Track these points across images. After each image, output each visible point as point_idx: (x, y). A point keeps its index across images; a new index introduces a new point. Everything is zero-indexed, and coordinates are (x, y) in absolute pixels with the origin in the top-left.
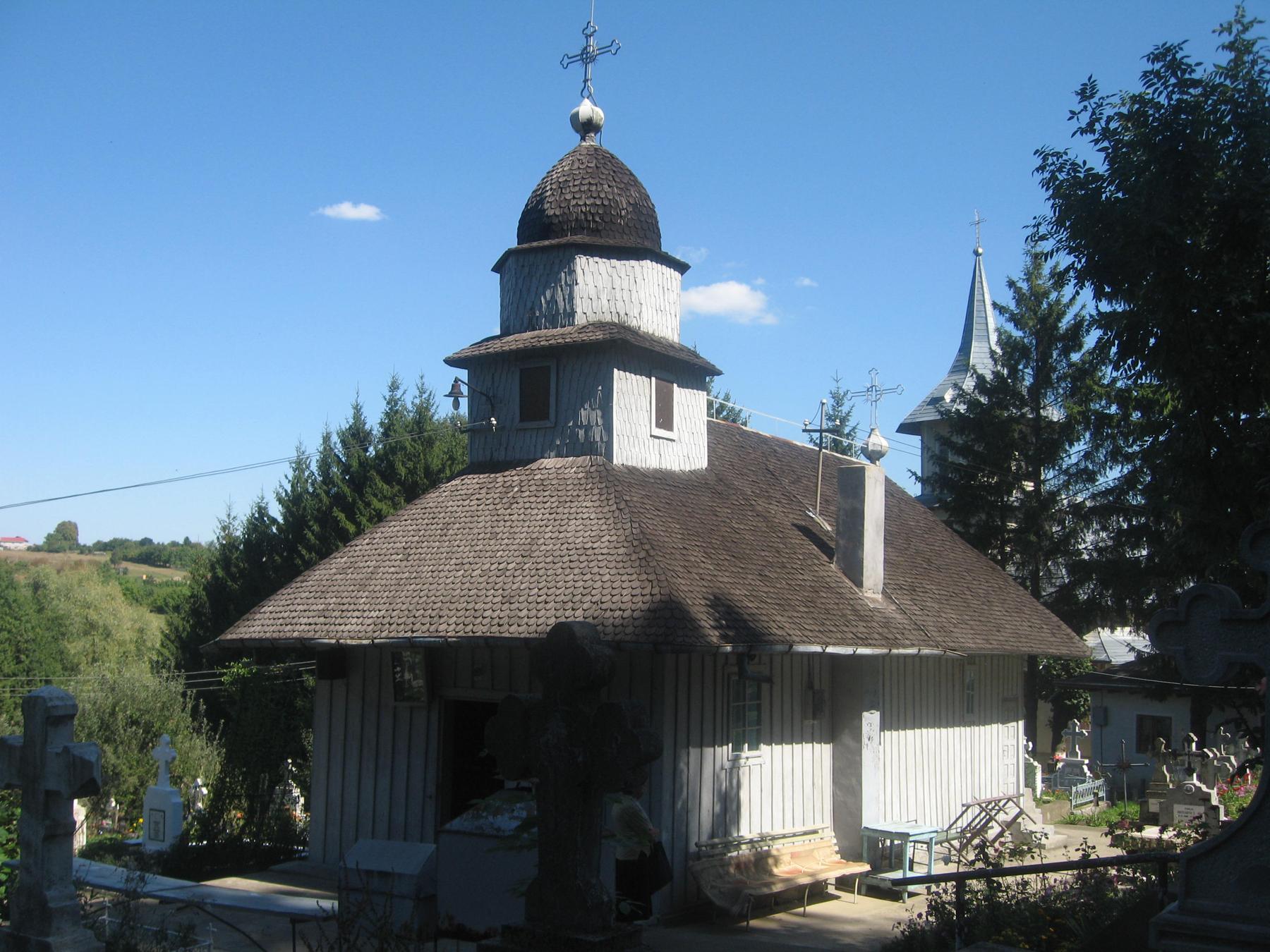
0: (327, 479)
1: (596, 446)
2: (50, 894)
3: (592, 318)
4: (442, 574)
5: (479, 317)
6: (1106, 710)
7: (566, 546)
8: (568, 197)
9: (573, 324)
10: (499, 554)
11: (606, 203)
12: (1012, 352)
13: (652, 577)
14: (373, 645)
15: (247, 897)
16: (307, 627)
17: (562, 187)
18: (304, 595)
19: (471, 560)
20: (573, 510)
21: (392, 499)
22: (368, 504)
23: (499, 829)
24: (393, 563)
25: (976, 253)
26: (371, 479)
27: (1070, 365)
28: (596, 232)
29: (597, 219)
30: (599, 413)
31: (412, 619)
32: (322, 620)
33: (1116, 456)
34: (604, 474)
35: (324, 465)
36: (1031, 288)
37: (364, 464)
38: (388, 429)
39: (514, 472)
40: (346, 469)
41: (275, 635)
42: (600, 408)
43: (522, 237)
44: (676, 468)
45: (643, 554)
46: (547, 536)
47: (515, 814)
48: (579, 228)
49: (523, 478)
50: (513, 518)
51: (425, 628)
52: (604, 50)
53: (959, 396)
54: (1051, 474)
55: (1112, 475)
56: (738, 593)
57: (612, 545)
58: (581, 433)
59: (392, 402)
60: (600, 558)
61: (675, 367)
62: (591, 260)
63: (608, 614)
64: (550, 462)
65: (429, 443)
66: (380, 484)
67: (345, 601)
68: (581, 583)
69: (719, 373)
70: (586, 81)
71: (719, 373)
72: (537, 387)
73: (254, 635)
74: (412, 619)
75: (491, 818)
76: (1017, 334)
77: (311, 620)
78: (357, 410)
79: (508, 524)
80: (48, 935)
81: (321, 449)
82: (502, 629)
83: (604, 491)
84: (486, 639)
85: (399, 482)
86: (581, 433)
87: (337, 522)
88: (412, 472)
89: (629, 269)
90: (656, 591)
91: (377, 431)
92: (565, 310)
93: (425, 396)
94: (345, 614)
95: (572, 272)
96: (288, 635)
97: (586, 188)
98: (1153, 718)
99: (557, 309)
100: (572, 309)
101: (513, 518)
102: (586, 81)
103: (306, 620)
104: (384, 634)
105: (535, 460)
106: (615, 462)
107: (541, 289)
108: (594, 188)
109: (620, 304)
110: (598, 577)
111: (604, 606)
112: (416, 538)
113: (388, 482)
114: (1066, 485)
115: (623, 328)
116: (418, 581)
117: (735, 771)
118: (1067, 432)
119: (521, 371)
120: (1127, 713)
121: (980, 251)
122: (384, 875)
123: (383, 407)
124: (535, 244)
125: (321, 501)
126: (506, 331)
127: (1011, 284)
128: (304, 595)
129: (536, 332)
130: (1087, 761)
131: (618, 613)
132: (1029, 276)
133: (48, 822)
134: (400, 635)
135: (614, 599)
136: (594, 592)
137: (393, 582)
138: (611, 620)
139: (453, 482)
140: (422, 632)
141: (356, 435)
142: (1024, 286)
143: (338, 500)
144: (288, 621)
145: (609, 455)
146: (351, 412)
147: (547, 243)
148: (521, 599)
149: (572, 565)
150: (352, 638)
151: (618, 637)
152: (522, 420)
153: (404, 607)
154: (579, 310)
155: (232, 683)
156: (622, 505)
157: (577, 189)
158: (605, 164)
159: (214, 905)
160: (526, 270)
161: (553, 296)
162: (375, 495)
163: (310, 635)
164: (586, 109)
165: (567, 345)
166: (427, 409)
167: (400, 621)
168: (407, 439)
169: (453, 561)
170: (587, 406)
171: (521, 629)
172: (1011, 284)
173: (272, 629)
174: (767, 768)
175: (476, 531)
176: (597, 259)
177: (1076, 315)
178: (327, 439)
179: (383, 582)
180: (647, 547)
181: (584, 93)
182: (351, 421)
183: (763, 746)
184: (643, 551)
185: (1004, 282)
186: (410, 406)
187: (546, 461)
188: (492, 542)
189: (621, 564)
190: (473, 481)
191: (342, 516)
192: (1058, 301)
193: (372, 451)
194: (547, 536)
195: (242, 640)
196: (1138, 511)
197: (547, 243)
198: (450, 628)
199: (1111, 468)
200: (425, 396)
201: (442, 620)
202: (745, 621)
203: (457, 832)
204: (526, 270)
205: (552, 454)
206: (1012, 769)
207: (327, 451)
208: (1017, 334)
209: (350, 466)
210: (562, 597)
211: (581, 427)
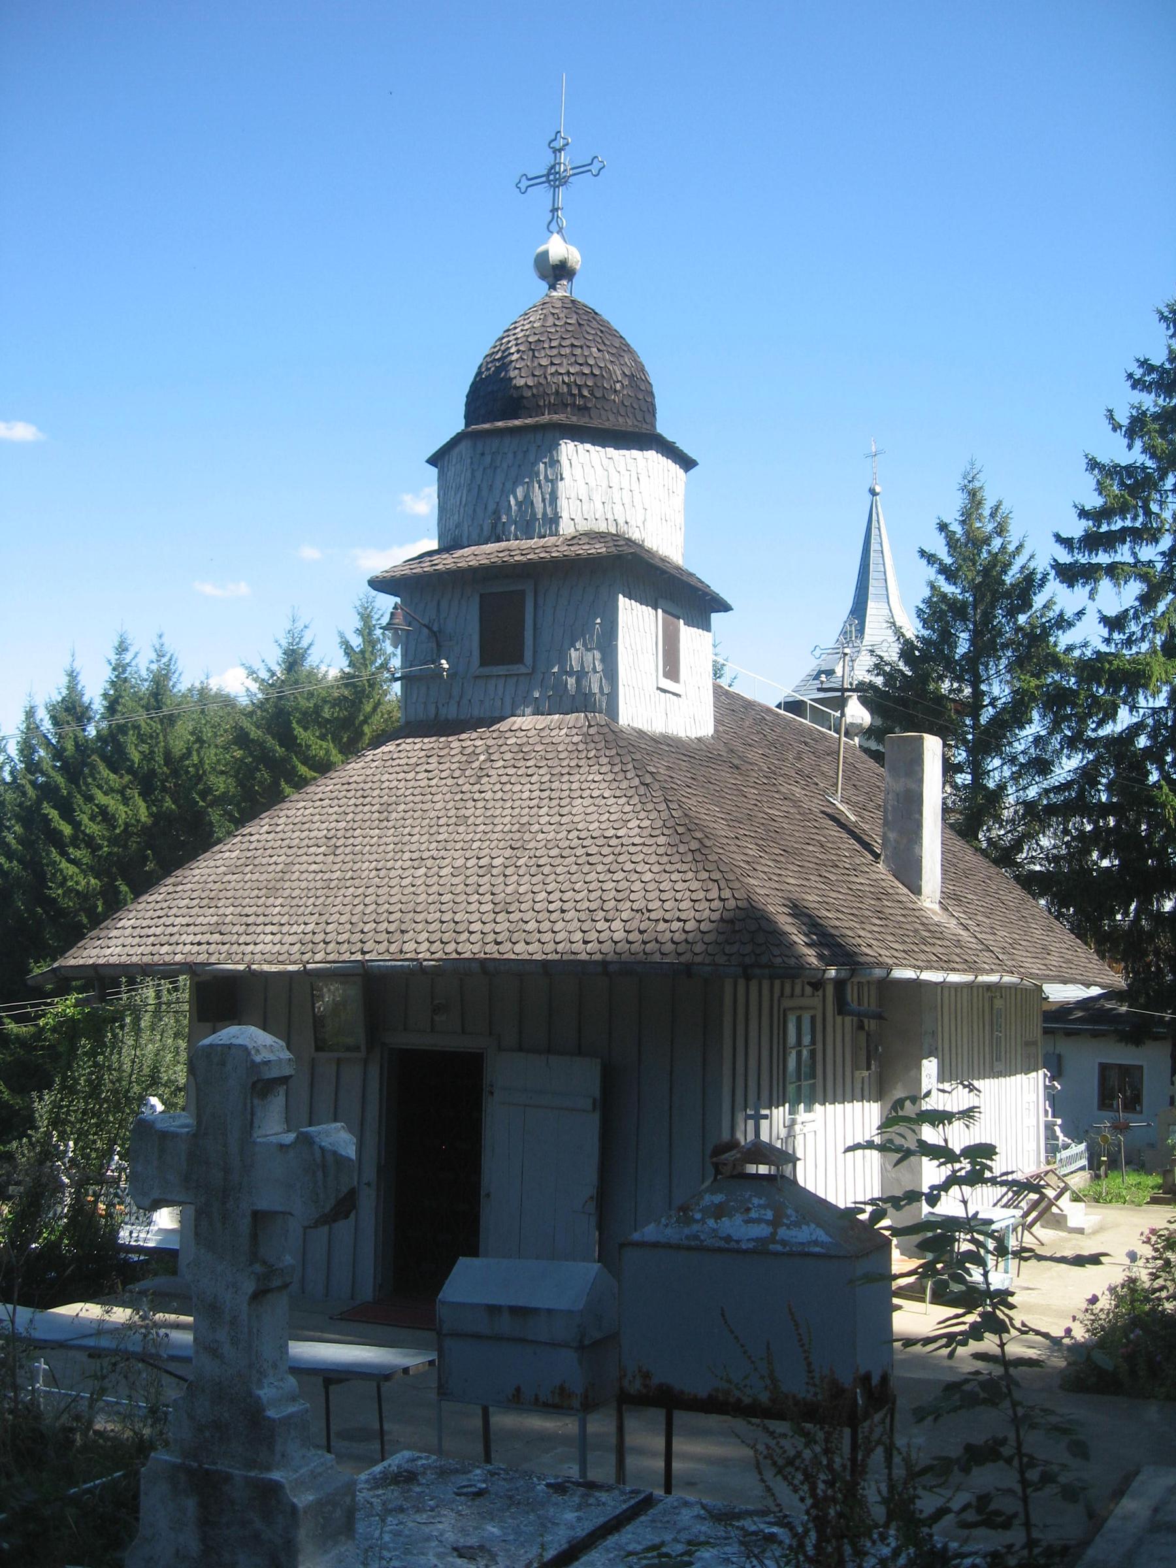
0: (32, 767)
1: (592, 702)
2: (265, 1393)
3: (583, 527)
4: (393, 873)
5: (409, 526)
6: (1059, 1057)
7: (574, 834)
8: (544, 362)
9: (557, 534)
10: (476, 845)
11: (597, 372)
12: (939, 612)
13: (716, 875)
14: (306, 972)
15: (101, 1329)
16: (196, 948)
17: (532, 349)
18: (183, 903)
19: (435, 853)
20: (574, 786)
21: (122, 792)
22: (89, 799)
23: (728, 1238)
24: (312, 859)
25: (873, 493)
26: (93, 767)
27: (1019, 629)
28: (583, 410)
29: (586, 393)
30: (598, 655)
31: (359, 936)
32: (217, 937)
33: (1073, 743)
34: (610, 737)
35: (27, 749)
36: (967, 533)
37: (82, 747)
38: (112, 706)
39: (474, 735)
40: (58, 753)
41: (146, 959)
42: (597, 648)
43: (470, 418)
44: (682, 734)
45: (694, 845)
46: (543, 820)
47: (753, 1214)
48: (561, 404)
49: (490, 742)
50: (488, 795)
51: (382, 948)
52: (581, 169)
53: (877, 666)
54: (997, 762)
55: (1068, 766)
56: (811, 899)
57: (645, 833)
58: (571, 681)
59: (120, 668)
60: (632, 849)
61: (687, 599)
62: (580, 446)
63: (662, 926)
64: (526, 722)
65: (171, 720)
66: (105, 772)
67: (247, 910)
68: (611, 885)
69: (726, 608)
70: (555, 210)
71: (726, 608)
72: (500, 622)
73: (112, 960)
74: (359, 936)
75: (711, 1222)
76: (949, 589)
77: (198, 938)
78: (72, 676)
79: (480, 804)
80: (268, 1469)
81: (23, 727)
82: (502, 948)
83: (617, 760)
84: (483, 962)
85: (131, 771)
86: (571, 681)
87: (46, 820)
88: (148, 757)
89: (630, 461)
90: (726, 894)
91: (99, 706)
92: (545, 514)
93: (164, 660)
94: (251, 929)
95: (554, 463)
96: (167, 959)
97: (568, 350)
98: (1120, 1065)
99: (534, 514)
100: (556, 513)
101: (488, 795)
102: (555, 210)
103: (191, 938)
104: (318, 957)
105: (502, 719)
106: (621, 722)
107: (509, 485)
108: (578, 351)
109: (618, 508)
110: (635, 877)
111: (653, 916)
112: (343, 824)
113: (115, 771)
114: (1015, 777)
115: (616, 538)
116: (357, 882)
117: (790, 1140)
118: (1015, 715)
119: (481, 596)
120: (1089, 1058)
121: (878, 489)
122: (519, 1312)
123: (107, 674)
124: (500, 424)
125: (24, 794)
126: (449, 544)
127: (943, 527)
128: (183, 903)
129: (503, 544)
130: (1059, 1121)
131: (676, 925)
132: (967, 516)
133: (258, 1268)
134: (346, 957)
135: (667, 906)
136: (633, 897)
137: (319, 884)
138: (668, 935)
139: (384, 749)
140: (378, 953)
141: (71, 710)
142: (956, 528)
143: (48, 792)
144: (164, 939)
145: (612, 710)
146: (65, 680)
147: (517, 422)
148: (523, 907)
149: (592, 860)
150: (270, 963)
151: (683, 959)
152: (484, 663)
153: (343, 919)
154: (565, 515)
155: (54, 1030)
156: (648, 779)
157: (555, 352)
158: (584, 320)
159: (173, 1358)
160: (488, 459)
161: (527, 496)
162: (100, 787)
163: (202, 958)
164: (557, 248)
165: (530, 564)
166: (167, 677)
167: (341, 938)
168: (141, 717)
169: (407, 856)
170: (578, 645)
171: (531, 948)
172: (943, 527)
173: (140, 950)
174: (821, 1134)
175: (433, 814)
176: (588, 446)
177: (1023, 567)
178: (30, 713)
179: (304, 885)
180: (699, 835)
181: (553, 223)
182: (65, 692)
183: (817, 1106)
184: (691, 842)
185: (933, 526)
186: (144, 673)
187: (519, 720)
188: (461, 829)
189: (665, 859)
190: (413, 747)
191: (54, 814)
192: (1003, 547)
193: (92, 731)
194: (543, 820)
195: (95, 966)
196: (1105, 810)
197: (517, 422)
198: (421, 946)
199: (1069, 757)
200: (164, 660)
201: (407, 937)
202: (833, 936)
203: (655, 1245)
204: (488, 459)
205: (528, 710)
206: (1033, 1131)
207: (31, 727)
208: (949, 589)
209: (64, 749)
210: (586, 904)
211: (570, 673)
